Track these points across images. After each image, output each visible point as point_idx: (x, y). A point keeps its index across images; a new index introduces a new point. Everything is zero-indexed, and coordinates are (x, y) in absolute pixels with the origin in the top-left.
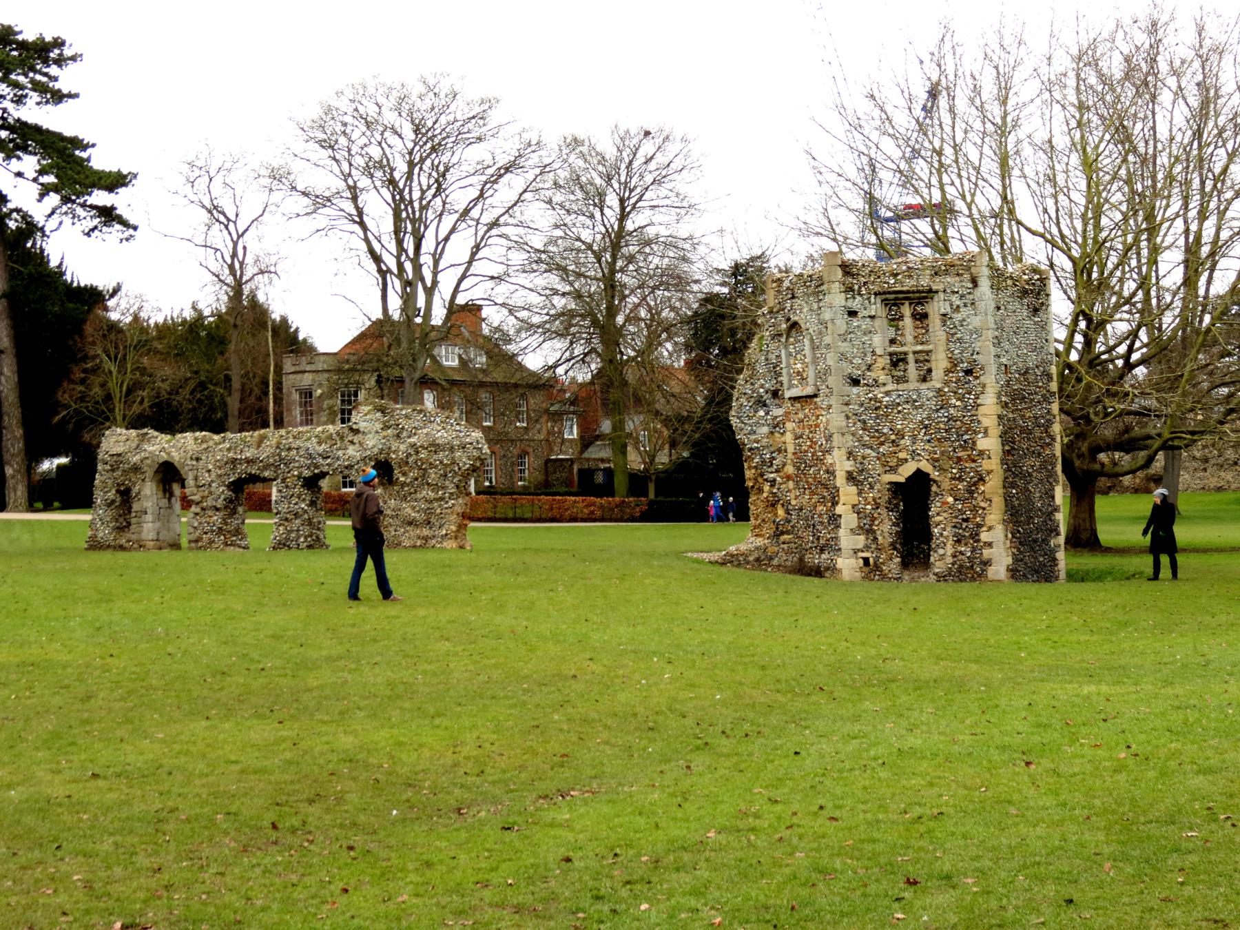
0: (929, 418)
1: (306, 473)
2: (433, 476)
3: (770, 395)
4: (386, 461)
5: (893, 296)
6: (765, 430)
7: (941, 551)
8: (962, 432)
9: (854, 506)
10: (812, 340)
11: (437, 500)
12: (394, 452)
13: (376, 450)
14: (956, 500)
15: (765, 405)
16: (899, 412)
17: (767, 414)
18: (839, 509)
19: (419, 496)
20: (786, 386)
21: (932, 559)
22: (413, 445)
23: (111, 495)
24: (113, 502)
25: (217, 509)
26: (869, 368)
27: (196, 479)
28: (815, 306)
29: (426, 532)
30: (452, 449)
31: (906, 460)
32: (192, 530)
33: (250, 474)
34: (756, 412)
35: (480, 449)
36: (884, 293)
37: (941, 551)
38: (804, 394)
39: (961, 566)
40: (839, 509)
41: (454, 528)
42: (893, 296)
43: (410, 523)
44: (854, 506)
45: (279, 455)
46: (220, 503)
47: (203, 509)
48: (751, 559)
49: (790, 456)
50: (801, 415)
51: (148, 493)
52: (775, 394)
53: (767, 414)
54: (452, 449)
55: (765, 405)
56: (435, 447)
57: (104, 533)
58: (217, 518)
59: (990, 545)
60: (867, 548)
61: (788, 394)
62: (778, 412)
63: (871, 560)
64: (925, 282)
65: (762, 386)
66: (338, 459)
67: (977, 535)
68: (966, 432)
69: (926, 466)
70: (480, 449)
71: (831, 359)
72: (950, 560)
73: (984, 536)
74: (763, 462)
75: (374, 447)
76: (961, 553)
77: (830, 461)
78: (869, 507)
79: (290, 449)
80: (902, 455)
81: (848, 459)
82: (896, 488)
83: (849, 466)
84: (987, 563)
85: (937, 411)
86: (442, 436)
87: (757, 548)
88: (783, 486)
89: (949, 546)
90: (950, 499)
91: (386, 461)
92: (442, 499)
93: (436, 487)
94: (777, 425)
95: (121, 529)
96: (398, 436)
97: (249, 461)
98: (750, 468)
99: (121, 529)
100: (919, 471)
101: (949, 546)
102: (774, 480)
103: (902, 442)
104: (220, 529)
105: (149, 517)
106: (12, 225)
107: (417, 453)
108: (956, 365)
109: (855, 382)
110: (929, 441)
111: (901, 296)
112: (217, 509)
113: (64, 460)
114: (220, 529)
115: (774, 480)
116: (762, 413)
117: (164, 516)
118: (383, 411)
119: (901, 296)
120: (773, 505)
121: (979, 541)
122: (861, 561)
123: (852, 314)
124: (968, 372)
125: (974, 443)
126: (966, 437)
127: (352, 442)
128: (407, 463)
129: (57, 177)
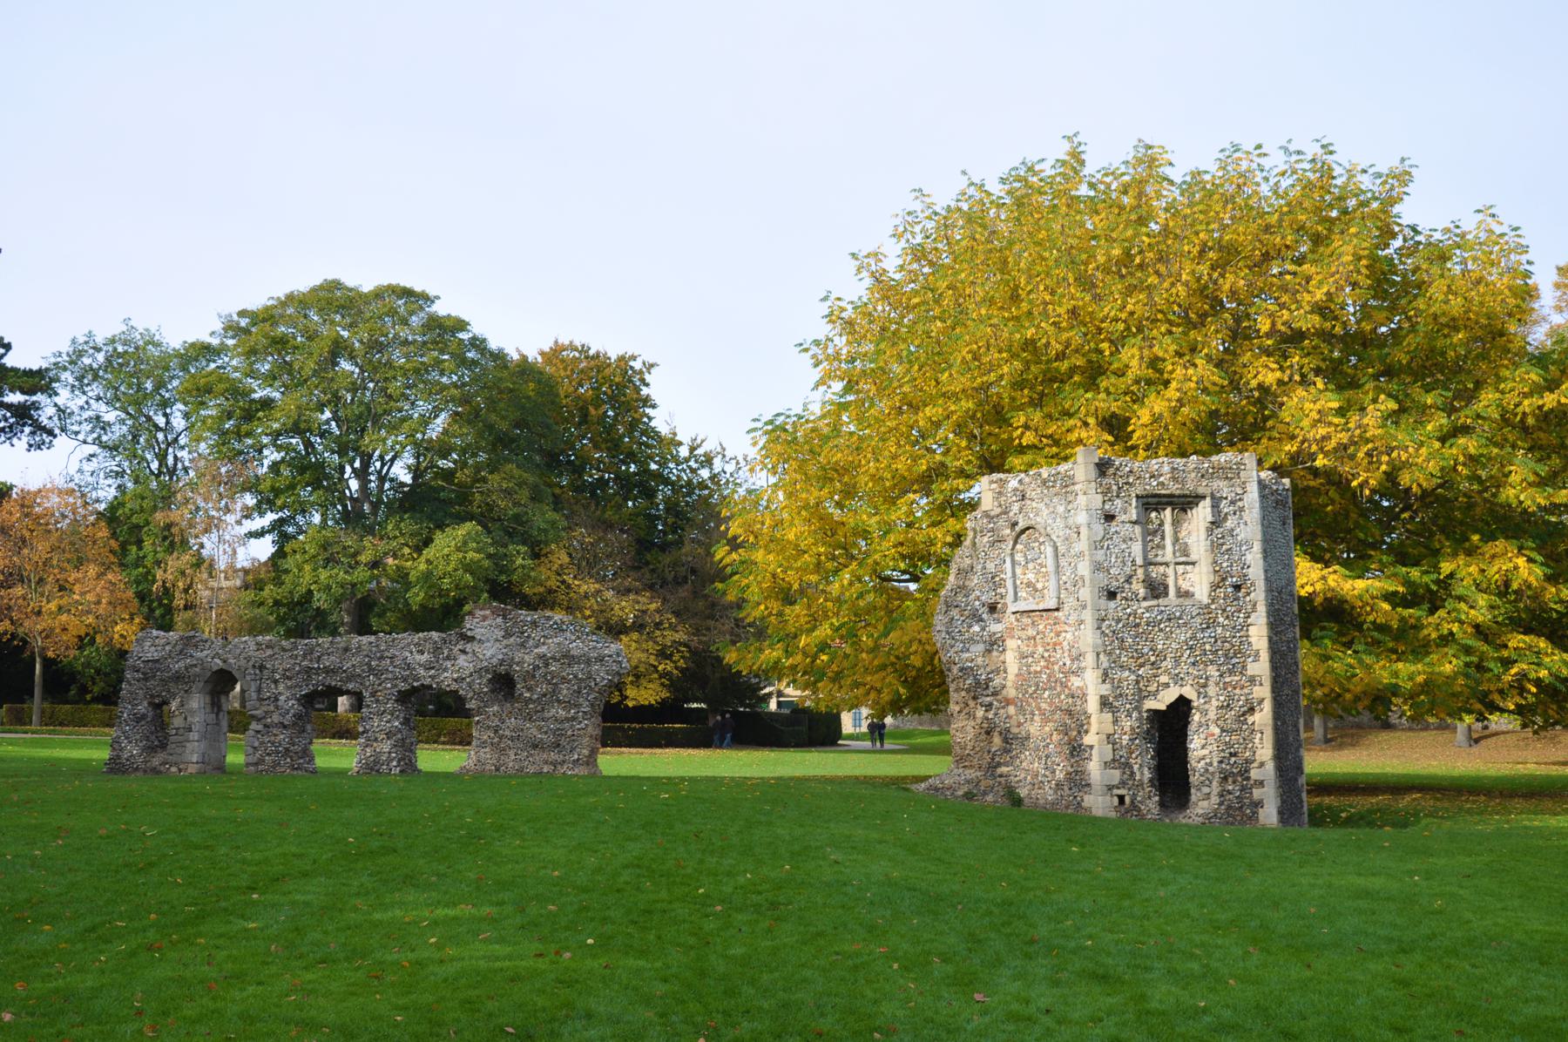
1: (403, 686)
2: (565, 691)
3: (986, 609)
4: (507, 674)
6: (981, 647)
7: (1206, 790)
8: (1234, 657)
11: (568, 720)
12: (518, 664)
13: (495, 661)
14: (1223, 731)
17: (983, 629)
18: (1088, 740)
19: (546, 715)
20: (1010, 598)
21: (1193, 798)
22: (542, 657)
23: (142, 708)
24: (144, 717)
25: (285, 727)
26: (1128, 580)
27: (259, 690)
28: (1061, 509)
29: (553, 756)
30: (588, 662)
31: (1167, 685)
32: (251, 750)
33: (329, 687)
35: (620, 662)
37: (1206, 790)
39: (1229, 807)
40: (1088, 740)
41: (585, 752)
43: (535, 746)
45: (368, 664)
46: (288, 720)
47: (266, 726)
49: (1011, 677)
50: (1031, 632)
51: (192, 708)
52: (993, 608)
54: (588, 662)
55: (982, 620)
56: (568, 658)
57: (132, 750)
58: (282, 737)
59: (1261, 784)
60: (1123, 784)
61: (1012, 608)
63: (1127, 799)
64: (1190, 486)
65: (978, 598)
66: (445, 670)
68: (1235, 656)
69: (1189, 692)
70: (620, 662)
72: (1215, 799)
73: (1255, 774)
74: (978, 683)
75: (493, 656)
76: (1229, 792)
79: (382, 658)
80: (1164, 679)
82: (1155, 713)
83: (1105, 689)
84: (1258, 804)
85: (1203, 630)
86: (577, 648)
87: (968, 782)
88: (1002, 711)
89: (1215, 784)
90: (1217, 731)
91: (507, 674)
92: (574, 719)
93: (568, 705)
95: (151, 750)
96: (522, 645)
97: (328, 671)
98: (957, 690)
99: (151, 750)
101: (1215, 784)
104: (287, 750)
105: (194, 736)
106: (1476, 538)
107: (547, 665)
108: (1224, 580)
109: (1112, 595)
112: (285, 727)
114: (287, 750)
115: (991, 705)
116: (976, 628)
117: (213, 736)
121: (1248, 779)
122: (1116, 800)
123: (1109, 518)
124: (1237, 588)
126: (1234, 661)
127: (463, 652)
128: (534, 676)
129: (337, 364)
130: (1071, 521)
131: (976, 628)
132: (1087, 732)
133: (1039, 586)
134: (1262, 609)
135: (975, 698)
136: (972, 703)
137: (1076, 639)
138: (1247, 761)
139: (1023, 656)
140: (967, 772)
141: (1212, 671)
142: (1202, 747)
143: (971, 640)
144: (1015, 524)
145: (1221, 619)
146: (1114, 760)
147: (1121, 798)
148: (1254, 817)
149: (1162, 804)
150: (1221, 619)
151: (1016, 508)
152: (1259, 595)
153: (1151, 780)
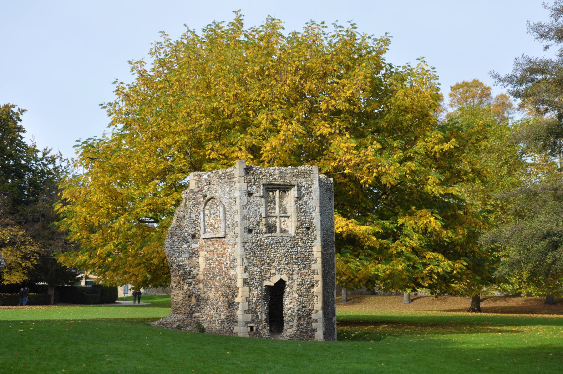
0: (287, 252)
3: (190, 237)
5: (271, 186)
6: (187, 255)
7: (291, 324)
8: (305, 261)
9: (247, 298)
10: (224, 208)
14: (299, 296)
16: (272, 248)
17: (189, 246)
18: (237, 300)
21: (285, 328)
26: (258, 224)
28: (227, 189)
31: (275, 274)
34: (182, 245)
37: (291, 324)
39: (301, 332)
42: (271, 186)
44: (247, 298)
49: (201, 270)
50: (212, 248)
52: (193, 236)
53: (189, 246)
59: (316, 321)
60: (253, 321)
61: (203, 236)
62: (195, 246)
63: (254, 328)
64: (288, 180)
65: (187, 232)
67: (310, 315)
69: (285, 277)
71: (238, 218)
72: (295, 328)
73: (313, 316)
76: (302, 325)
77: (232, 273)
78: (255, 299)
80: (273, 271)
83: (246, 276)
84: (315, 330)
85: (292, 248)
87: (179, 320)
88: (196, 286)
89: (295, 321)
90: (297, 296)
94: (194, 253)
98: (175, 276)
100: (281, 280)
101: (295, 321)
103: (273, 264)
108: (302, 225)
109: (250, 231)
110: (287, 264)
115: (191, 283)
116: (185, 246)
118: (528, 137)
120: (189, 297)
121: (310, 318)
122: (249, 329)
123: (250, 194)
124: (308, 229)
125: (310, 266)
130: (232, 195)
131: (185, 246)
132: (236, 296)
133: (216, 226)
134: (319, 238)
135: (183, 280)
136: (182, 282)
137: (233, 252)
139: (207, 260)
140: (179, 316)
141: (296, 267)
142: (290, 304)
143: (183, 252)
145: (300, 243)
146: (249, 310)
147: (252, 328)
149: (270, 331)
150: (300, 243)
151: (206, 188)
152: (318, 232)
153: (266, 319)
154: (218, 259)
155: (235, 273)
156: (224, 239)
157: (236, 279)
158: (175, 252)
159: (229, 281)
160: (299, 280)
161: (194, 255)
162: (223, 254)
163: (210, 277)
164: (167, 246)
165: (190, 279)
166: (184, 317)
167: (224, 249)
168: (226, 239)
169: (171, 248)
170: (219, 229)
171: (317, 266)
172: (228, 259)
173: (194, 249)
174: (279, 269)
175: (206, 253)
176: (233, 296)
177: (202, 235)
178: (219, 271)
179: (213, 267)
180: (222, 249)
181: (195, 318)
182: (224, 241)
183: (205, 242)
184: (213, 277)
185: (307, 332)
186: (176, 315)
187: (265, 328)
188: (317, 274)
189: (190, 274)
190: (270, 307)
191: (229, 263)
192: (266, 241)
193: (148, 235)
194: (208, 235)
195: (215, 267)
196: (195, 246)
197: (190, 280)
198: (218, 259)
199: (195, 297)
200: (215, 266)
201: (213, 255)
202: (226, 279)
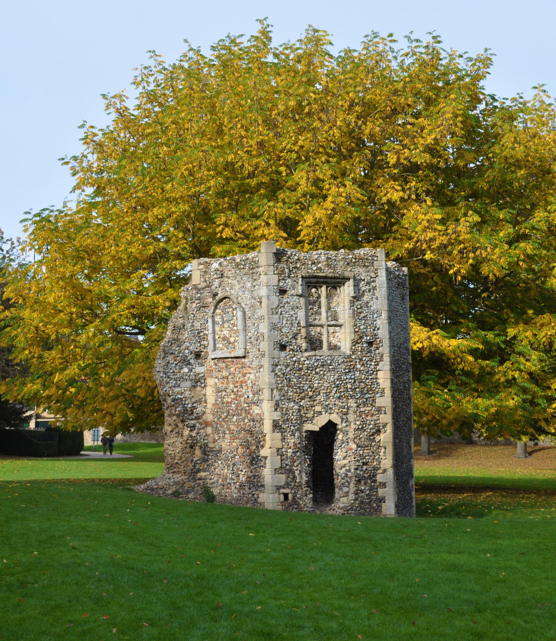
0: (339, 379)
3: (193, 356)
6: (188, 384)
7: (345, 489)
8: (366, 393)
9: (278, 450)
10: (244, 313)
14: (358, 446)
15: (190, 364)
16: (317, 373)
17: (190, 371)
18: (264, 452)
21: (337, 495)
26: (295, 337)
28: (249, 285)
31: (320, 413)
34: (181, 368)
36: (309, 277)
37: (345, 489)
38: (233, 355)
39: (362, 502)
40: (264, 452)
44: (278, 450)
48: (170, 492)
49: (209, 406)
50: (225, 373)
52: (198, 355)
55: (190, 364)
59: (384, 485)
60: (287, 485)
61: (212, 355)
63: (290, 496)
64: (339, 271)
65: (187, 348)
67: (374, 476)
68: (368, 392)
69: (335, 418)
72: (352, 496)
73: (380, 478)
74: (185, 410)
76: (362, 491)
80: (318, 408)
81: (276, 410)
83: (277, 416)
84: (382, 500)
85: (346, 373)
87: (176, 483)
89: (352, 485)
90: (354, 446)
94: (199, 381)
98: (170, 415)
101: (352, 485)
102: (194, 426)
108: (361, 338)
109: (283, 347)
110: (339, 398)
111: (322, 280)
113: (25, 415)
115: (194, 426)
116: (186, 370)
119: (322, 280)
120: (191, 447)
121: (375, 481)
122: (282, 497)
123: (283, 292)
124: (370, 344)
125: (374, 401)
130: (255, 294)
131: (186, 370)
132: (263, 446)
133: (232, 340)
134: (387, 359)
135: (183, 421)
136: (180, 425)
137: (257, 379)
138: (375, 469)
140: (176, 476)
141: (352, 403)
142: (343, 459)
143: (182, 379)
144: (216, 295)
145: (359, 366)
146: (281, 467)
148: (378, 509)
150: (359, 366)
151: (216, 283)
152: (385, 349)
153: (307, 482)
154: (235, 390)
155: (260, 412)
156: (243, 360)
157: (261, 421)
158: (171, 379)
159: (252, 423)
160: (358, 423)
161: (199, 384)
162: (242, 382)
163: (223, 416)
164: (158, 369)
165: (192, 419)
166: (184, 477)
167: (244, 375)
168: (246, 360)
169: (165, 373)
170: (236, 344)
171: (385, 401)
172: (249, 390)
173: (199, 374)
174: (327, 406)
175: (216, 380)
176: (257, 447)
177: (210, 353)
178: (237, 409)
179: (228, 403)
180: (240, 375)
181: (200, 479)
182: (243, 363)
183: (215, 364)
184: (226, 417)
185: (370, 502)
186: (171, 475)
187: (306, 495)
188: (385, 413)
189: (192, 413)
190: (314, 463)
191: (251, 396)
192: (307, 362)
193: (130, 352)
194: (219, 354)
195: (231, 403)
196: (199, 370)
197: (193, 422)
198: (235, 390)
199: (201, 447)
200: (229, 400)
201: (228, 383)
202: (246, 421)
